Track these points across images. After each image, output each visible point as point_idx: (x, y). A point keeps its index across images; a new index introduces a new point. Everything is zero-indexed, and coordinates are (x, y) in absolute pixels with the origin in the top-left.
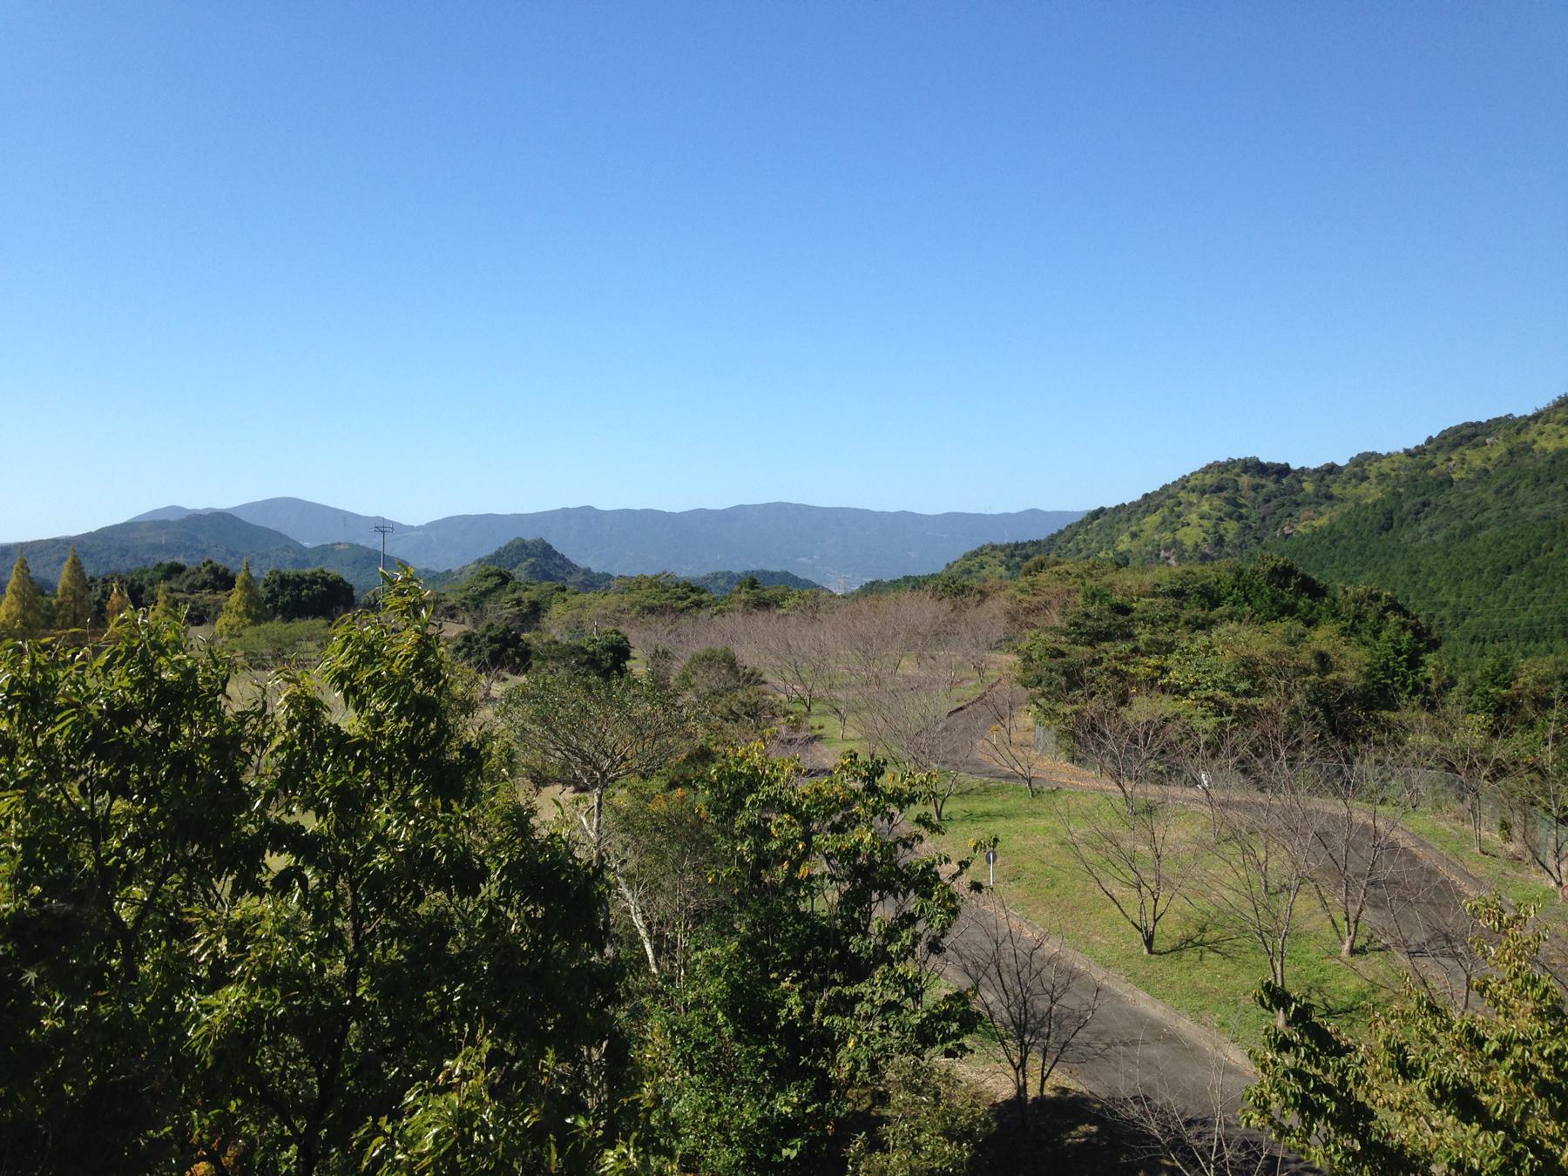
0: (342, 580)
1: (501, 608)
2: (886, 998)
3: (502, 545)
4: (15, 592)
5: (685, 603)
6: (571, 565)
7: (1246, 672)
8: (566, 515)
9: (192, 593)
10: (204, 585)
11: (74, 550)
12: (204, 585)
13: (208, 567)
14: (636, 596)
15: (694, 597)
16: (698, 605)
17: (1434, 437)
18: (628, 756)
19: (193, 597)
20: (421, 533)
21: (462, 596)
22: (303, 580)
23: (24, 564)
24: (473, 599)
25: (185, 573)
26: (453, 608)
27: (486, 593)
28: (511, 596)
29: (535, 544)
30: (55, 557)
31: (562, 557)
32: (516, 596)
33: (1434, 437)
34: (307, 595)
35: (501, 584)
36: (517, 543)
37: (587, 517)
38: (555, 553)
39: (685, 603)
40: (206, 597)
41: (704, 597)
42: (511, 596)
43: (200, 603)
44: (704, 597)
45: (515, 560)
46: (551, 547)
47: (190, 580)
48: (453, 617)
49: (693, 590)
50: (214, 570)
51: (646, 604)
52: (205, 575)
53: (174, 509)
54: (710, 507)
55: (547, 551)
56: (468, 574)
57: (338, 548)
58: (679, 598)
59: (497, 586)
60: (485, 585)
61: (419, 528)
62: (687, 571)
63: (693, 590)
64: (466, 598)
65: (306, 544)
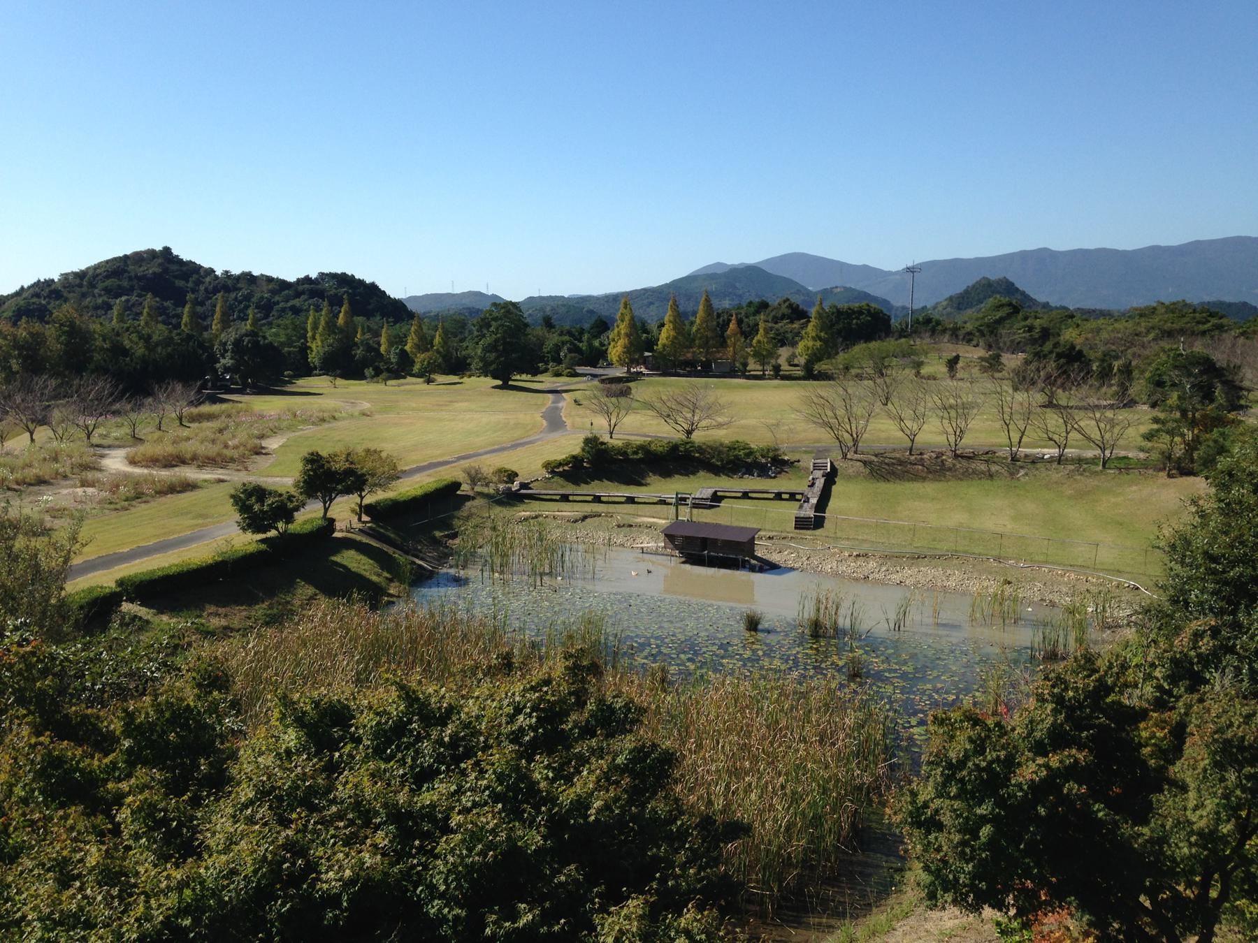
0: (882, 312)
1: (1014, 334)
2: (913, 844)
3: (970, 285)
4: (670, 322)
5: (1206, 326)
6: (1032, 300)
7: (766, 663)
8: (1024, 257)
9: (776, 323)
10: (783, 317)
11: (673, 294)
12: (783, 317)
13: (787, 304)
14: (1155, 320)
15: (1214, 321)
16: (1220, 328)
17: (26, 287)
18: (588, 556)
19: (776, 326)
20: (898, 277)
21: (978, 323)
22: (854, 312)
23: (707, 300)
24: (988, 326)
25: (770, 309)
26: (970, 333)
27: (1000, 321)
28: (1024, 323)
29: (1000, 282)
30: (645, 302)
31: (1023, 293)
32: (1028, 322)
33: (26, 287)
34: (857, 324)
35: (1012, 313)
36: (983, 282)
37: (1043, 258)
38: (1017, 289)
39: (1206, 326)
40: (784, 325)
41: (1224, 321)
42: (1024, 323)
43: (782, 331)
44: (1224, 321)
45: (981, 296)
46: (1013, 284)
47: (774, 313)
48: (969, 341)
49: (1212, 315)
50: (790, 306)
51: (1165, 327)
52: (784, 309)
53: (719, 264)
54: (1163, 243)
55: (1009, 287)
56: (940, 309)
57: (836, 291)
58: (1198, 323)
59: (1009, 316)
60: (999, 315)
61: (897, 273)
62: (1197, 296)
63: (1212, 315)
64: (981, 326)
65: (810, 288)
